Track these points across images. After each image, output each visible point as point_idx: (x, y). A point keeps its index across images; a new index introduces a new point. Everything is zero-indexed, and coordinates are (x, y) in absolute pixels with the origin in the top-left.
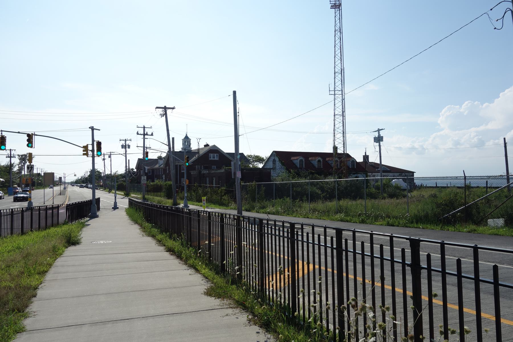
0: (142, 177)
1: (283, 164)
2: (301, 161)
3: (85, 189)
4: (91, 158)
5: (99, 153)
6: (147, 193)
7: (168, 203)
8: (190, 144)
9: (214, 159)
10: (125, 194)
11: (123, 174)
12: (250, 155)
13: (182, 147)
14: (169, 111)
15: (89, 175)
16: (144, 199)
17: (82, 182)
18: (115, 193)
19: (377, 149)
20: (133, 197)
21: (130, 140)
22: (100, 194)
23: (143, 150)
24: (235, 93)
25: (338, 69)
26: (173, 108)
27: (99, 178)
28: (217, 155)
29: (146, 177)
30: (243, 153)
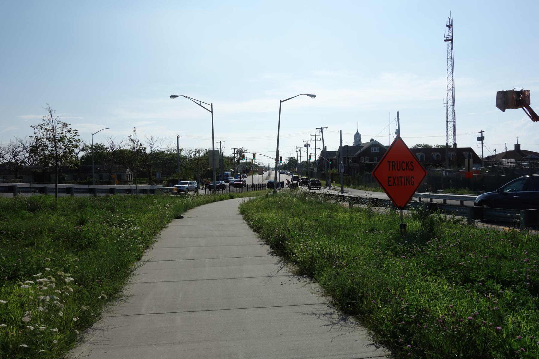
2: (422, 156)
5: (281, 162)
8: (360, 139)
9: (375, 152)
12: (420, 144)
13: (354, 141)
14: (324, 130)
15: (288, 162)
19: (480, 146)
24: (341, 131)
25: (450, 87)
26: (327, 128)
28: (378, 149)
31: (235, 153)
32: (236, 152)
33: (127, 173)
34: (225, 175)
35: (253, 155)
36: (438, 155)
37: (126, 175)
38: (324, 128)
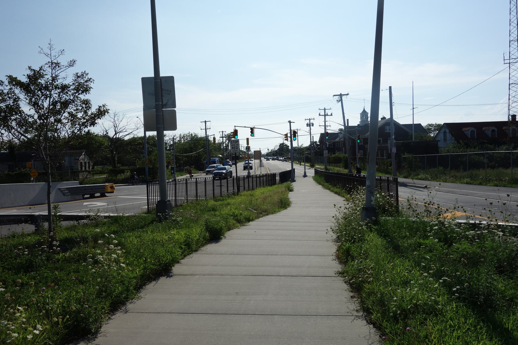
0: (324, 151)
1: (453, 135)
2: (472, 132)
3: (276, 161)
4: (290, 142)
6: (328, 164)
7: (346, 171)
10: (310, 165)
11: (308, 147)
12: (431, 124)
14: (344, 98)
16: (326, 169)
17: (275, 155)
18: (305, 165)
20: (318, 168)
21: (314, 119)
22: (296, 167)
23: (324, 128)
24: (390, 88)
26: (348, 94)
27: (287, 151)
29: (327, 151)
30: (420, 124)
31: (223, 137)
32: (224, 136)
33: (81, 161)
34: (212, 162)
35: (251, 130)
36: (493, 131)
37: (79, 164)
38: (344, 95)
